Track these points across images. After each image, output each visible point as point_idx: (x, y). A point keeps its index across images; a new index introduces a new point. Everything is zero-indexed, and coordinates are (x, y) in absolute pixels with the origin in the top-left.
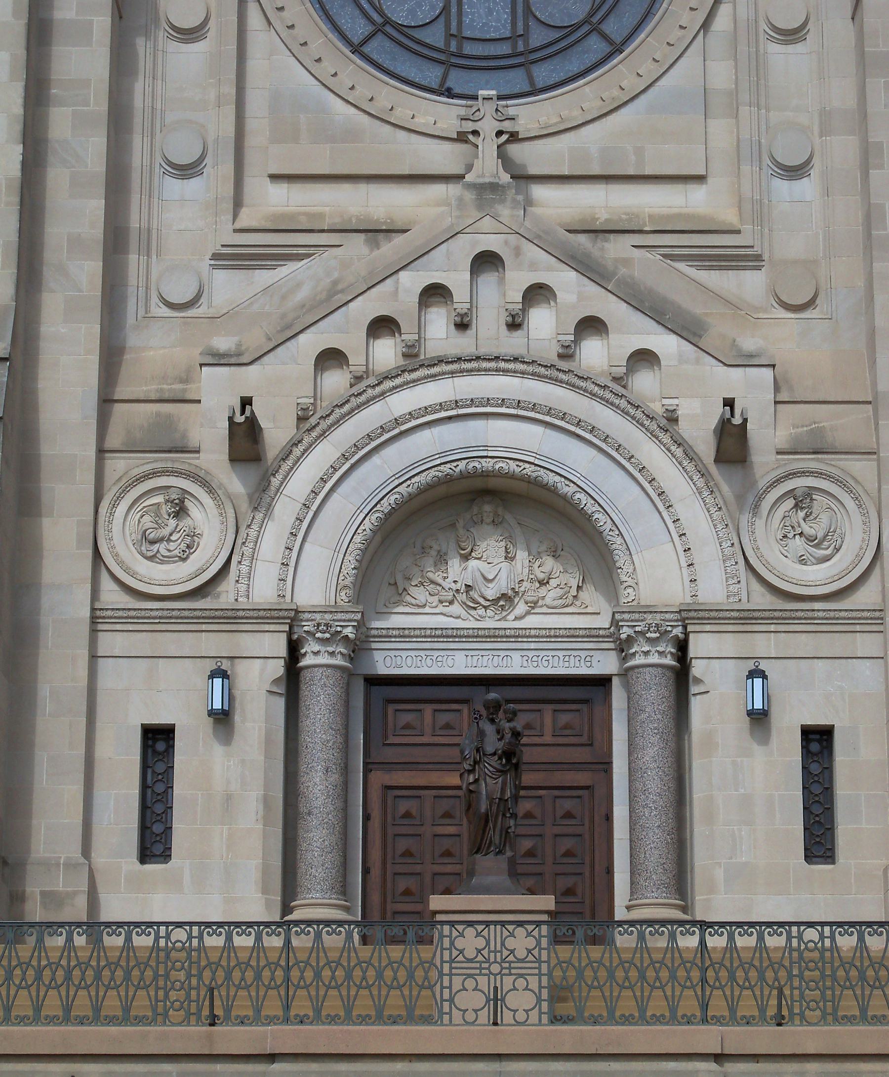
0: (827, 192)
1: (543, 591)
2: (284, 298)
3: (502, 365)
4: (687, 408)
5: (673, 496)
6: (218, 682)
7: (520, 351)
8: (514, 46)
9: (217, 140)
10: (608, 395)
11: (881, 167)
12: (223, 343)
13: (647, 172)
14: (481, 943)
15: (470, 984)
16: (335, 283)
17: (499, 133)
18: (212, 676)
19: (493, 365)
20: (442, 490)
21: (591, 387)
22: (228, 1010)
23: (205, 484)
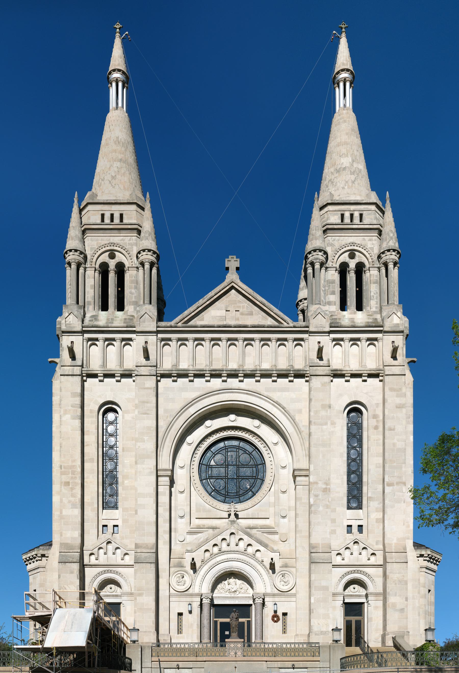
0: (289, 521)
1: (241, 590)
2: (199, 540)
3: (235, 552)
4: (265, 560)
5: (262, 574)
6: (190, 606)
7: (238, 550)
8: (237, 494)
9: (187, 512)
10: (252, 557)
11: (298, 517)
12: (189, 549)
13: (259, 517)
14: (234, 645)
15: (232, 651)
16: (207, 538)
17: (234, 511)
18: (189, 605)
19: (233, 552)
20: (225, 573)
21: (249, 556)
22: (199, 655)
23: (187, 573)
